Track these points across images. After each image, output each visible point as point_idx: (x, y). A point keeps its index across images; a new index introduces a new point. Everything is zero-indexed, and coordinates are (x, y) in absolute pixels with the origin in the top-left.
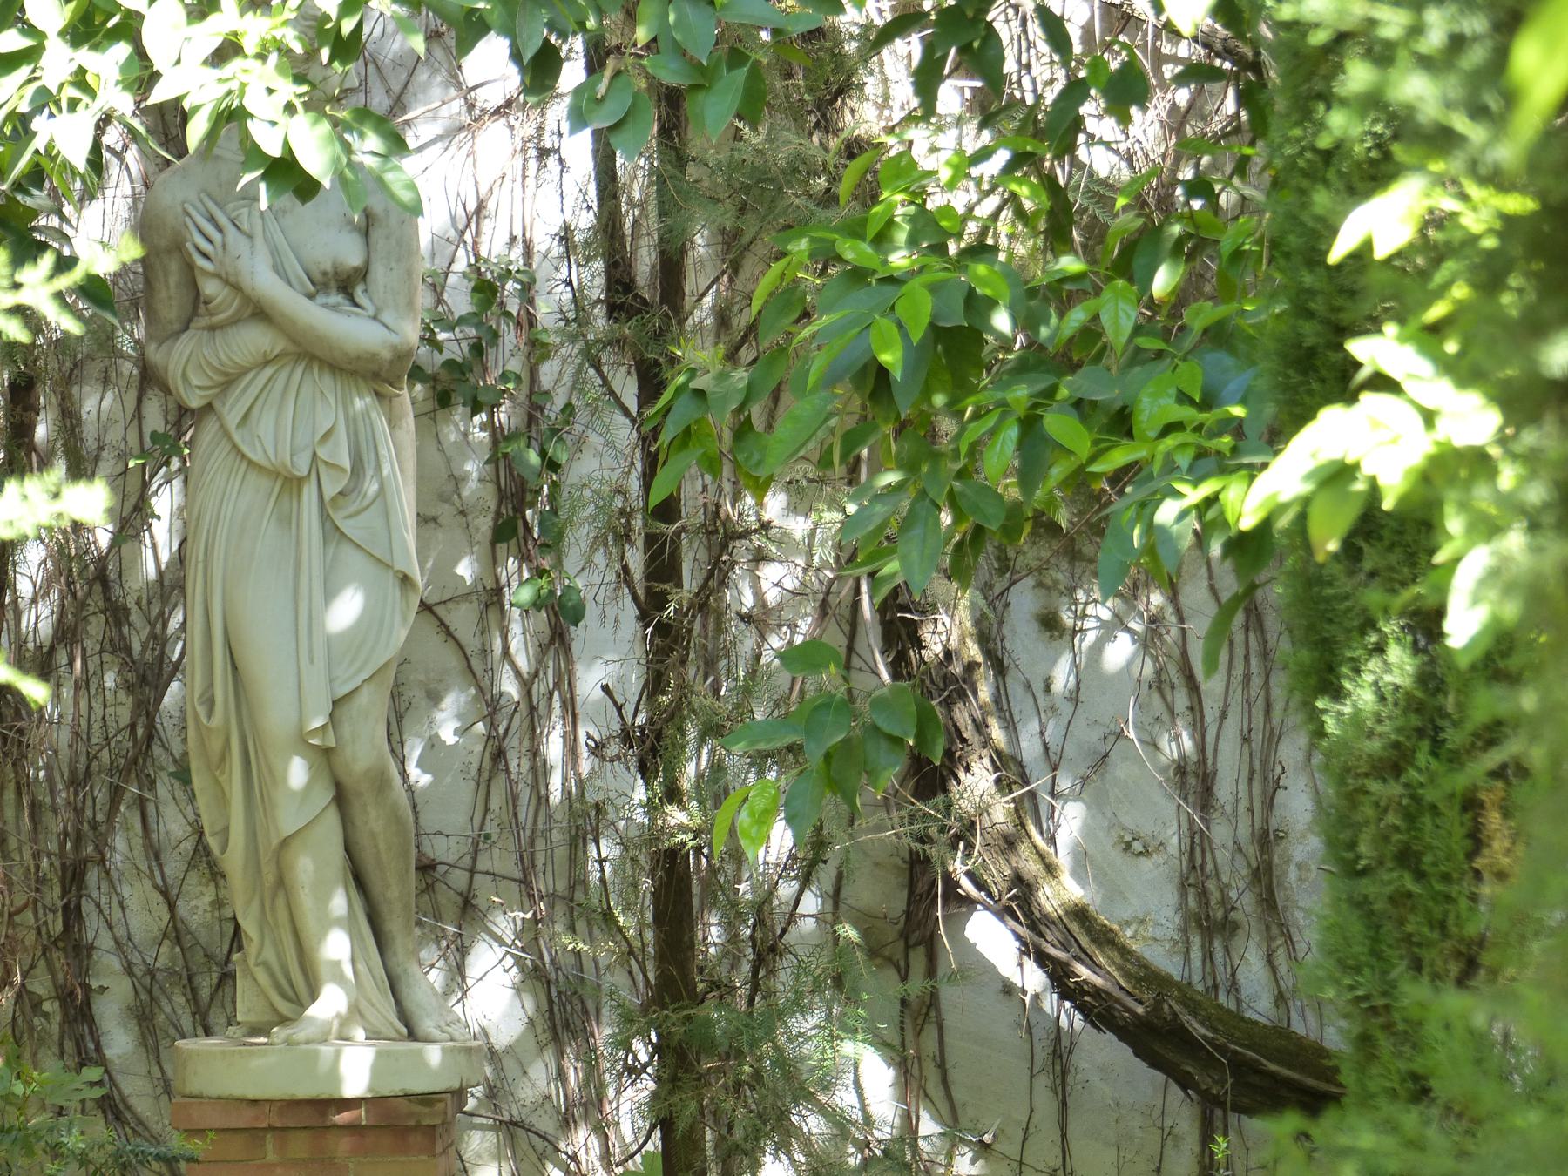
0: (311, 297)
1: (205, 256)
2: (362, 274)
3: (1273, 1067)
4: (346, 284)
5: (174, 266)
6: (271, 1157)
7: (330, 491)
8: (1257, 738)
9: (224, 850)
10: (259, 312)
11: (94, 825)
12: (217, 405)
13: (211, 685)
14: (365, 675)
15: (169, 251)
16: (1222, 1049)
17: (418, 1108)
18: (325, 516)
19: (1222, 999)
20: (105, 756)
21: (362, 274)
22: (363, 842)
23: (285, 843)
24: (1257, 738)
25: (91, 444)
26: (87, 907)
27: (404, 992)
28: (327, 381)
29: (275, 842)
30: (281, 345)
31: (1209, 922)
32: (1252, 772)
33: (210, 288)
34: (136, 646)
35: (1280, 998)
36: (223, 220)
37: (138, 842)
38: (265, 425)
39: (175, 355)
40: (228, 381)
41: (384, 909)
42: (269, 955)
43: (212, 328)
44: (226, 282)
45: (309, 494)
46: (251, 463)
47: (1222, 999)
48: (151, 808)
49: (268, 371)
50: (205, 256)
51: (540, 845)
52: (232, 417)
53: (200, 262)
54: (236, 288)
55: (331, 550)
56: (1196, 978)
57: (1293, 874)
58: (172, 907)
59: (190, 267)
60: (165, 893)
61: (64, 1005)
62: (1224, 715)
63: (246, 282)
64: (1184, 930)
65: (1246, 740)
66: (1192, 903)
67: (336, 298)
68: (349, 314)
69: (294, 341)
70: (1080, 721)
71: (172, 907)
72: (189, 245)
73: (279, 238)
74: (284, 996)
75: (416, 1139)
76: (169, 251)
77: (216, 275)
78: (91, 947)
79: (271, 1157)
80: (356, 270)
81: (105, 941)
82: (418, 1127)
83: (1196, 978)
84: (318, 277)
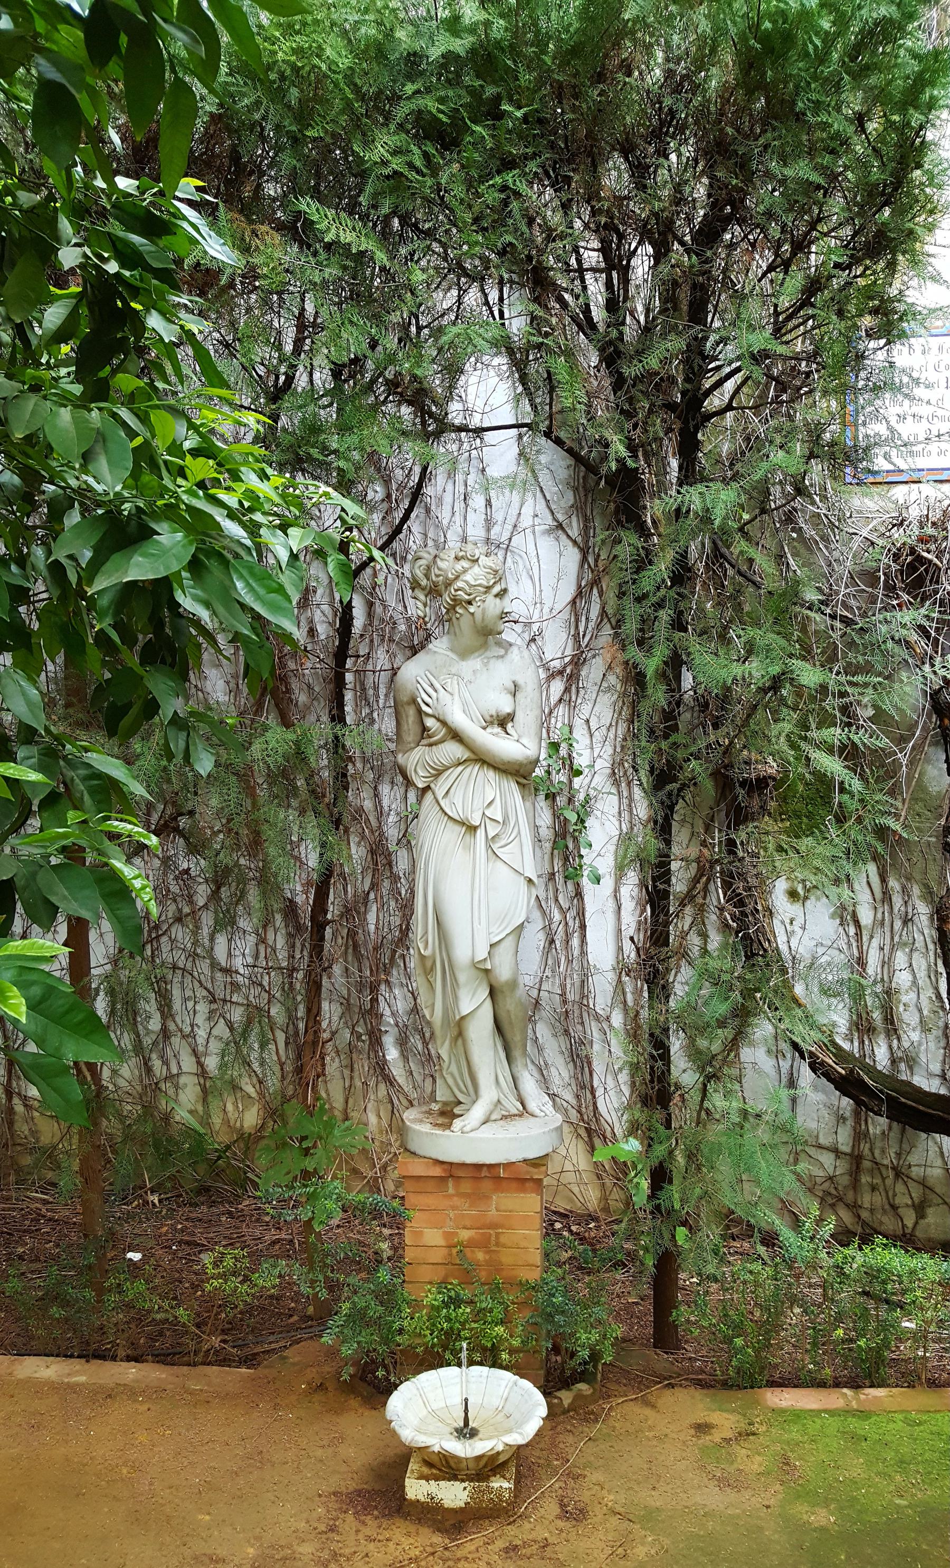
0: (484, 728)
1: (427, 705)
2: (511, 717)
3: (903, 1100)
4: (503, 722)
5: (411, 711)
6: (451, 1191)
7: (491, 834)
8: (887, 948)
9: (432, 1016)
10: (455, 735)
11: (385, 965)
12: (432, 786)
13: (426, 932)
14: (508, 931)
15: (408, 704)
16: (881, 1091)
17: (532, 1169)
18: (489, 847)
19: (867, 1060)
20: (389, 937)
21: (511, 717)
22: (503, 1015)
23: (463, 1018)
24: (887, 948)
25: (386, 809)
26: (380, 998)
27: (521, 1087)
28: (491, 774)
29: (458, 1017)
30: (467, 755)
31: (862, 1027)
32: (884, 962)
33: (430, 722)
34: (403, 892)
35: (894, 1061)
36: (437, 685)
37: (402, 971)
38: (457, 796)
39: (411, 759)
40: (438, 773)
41: (512, 1046)
42: (454, 1068)
43: (430, 745)
44: (438, 720)
45: (480, 833)
46: (449, 817)
47: (867, 1060)
48: (407, 960)
49: (460, 768)
50: (427, 705)
51: (568, 981)
52: (440, 793)
53: (425, 708)
54: (444, 723)
55: (490, 865)
56: (856, 1051)
57: (901, 1008)
58: (415, 999)
59: (420, 712)
60: (412, 993)
61: (370, 1038)
62: (872, 937)
63: (449, 720)
64: (850, 1029)
65: (882, 949)
66: (854, 1017)
67: (498, 730)
68: (504, 738)
69: (473, 752)
70: (805, 937)
71: (415, 999)
72: (419, 700)
73: (467, 695)
74: (462, 1092)
75: (529, 1185)
76: (408, 704)
77: (434, 716)
78: (382, 1015)
79: (451, 1191)
80: (509, 714)
81: (387, 1012)
82: (532, 1179)
83: (856, 1051)
84: (488, 718)
